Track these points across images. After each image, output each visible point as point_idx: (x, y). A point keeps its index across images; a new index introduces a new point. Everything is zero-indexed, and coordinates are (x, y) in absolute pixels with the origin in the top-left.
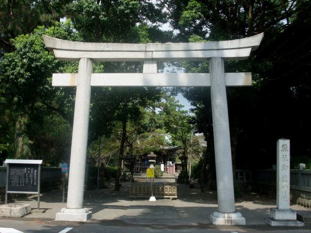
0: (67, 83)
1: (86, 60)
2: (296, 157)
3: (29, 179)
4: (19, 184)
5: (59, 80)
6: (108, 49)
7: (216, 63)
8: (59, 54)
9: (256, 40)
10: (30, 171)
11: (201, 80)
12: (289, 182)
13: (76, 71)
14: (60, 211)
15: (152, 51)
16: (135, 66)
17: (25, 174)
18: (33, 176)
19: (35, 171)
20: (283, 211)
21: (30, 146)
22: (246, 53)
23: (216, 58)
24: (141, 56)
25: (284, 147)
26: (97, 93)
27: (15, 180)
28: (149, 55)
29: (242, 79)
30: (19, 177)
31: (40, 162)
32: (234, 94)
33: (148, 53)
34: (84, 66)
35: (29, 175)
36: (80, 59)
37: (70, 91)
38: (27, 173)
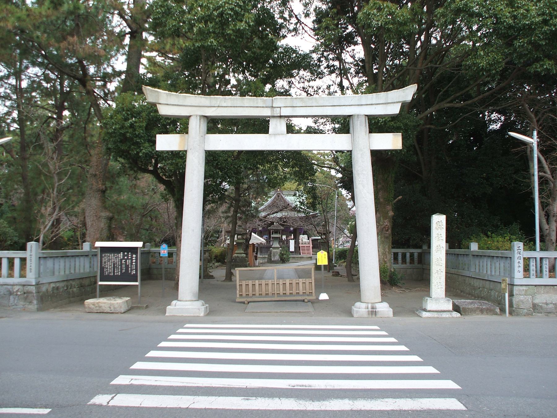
0: (175, 147)
1: (198, 118)
2: (454, 240)
3: (127, 267)
4: (114, 272)
5: (165, 142)
6: (225, 105)
7: (359, 123)
8: (164, 111)
9: (408, 93)
10: (128, 256)
11: (341, 142)
12: (444, 265)
13: (185, 130)
14: (170, 305)
15: (280, 107)
16: (259, 126)
17: (121, 260)
18: (132, 262)
19: (134, 256)
20: (437, 299)
21: (540, 73)
22: (395, 110)
23: (358, 115)
24: (266, 112)
25: (439, 223)
26: (213, 159)
27: (109, 267)
28: (277, 112)
29: (391, 142)
30: (114, 264)
31: (139, 244)
32: (379, 158)
33: (275, 109)
34: (196, 127)
35: (126, 262)
36: (190, 116)
37: (179, 158)
38: (124, 259)
